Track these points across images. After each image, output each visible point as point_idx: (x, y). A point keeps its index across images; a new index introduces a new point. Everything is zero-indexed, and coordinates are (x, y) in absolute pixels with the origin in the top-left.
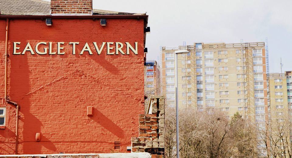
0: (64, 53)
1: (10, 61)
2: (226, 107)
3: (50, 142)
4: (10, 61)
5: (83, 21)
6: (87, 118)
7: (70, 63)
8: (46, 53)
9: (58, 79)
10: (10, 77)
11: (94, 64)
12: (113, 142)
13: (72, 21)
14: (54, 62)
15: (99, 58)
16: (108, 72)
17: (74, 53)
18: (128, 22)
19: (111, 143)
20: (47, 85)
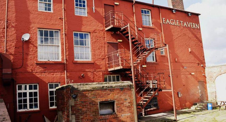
0: (179, 25)
1: (66, 37)
2: (217, 92)
3: (180, 62)
4: (66, 37)
5: (182, 13)
6: (189, 53)
7: (181, 30)
8: (173, 24)
9: (179, 36)
10: (68, 55)
11: (188, 31)
12: (197, 63)
13: (167, 10)
14: (176, 29)
15: (189, 28)
16: (192, 35)
17: (182, 26)
18: (179, 12)
19: (197, 63)
20: (176, 38)
